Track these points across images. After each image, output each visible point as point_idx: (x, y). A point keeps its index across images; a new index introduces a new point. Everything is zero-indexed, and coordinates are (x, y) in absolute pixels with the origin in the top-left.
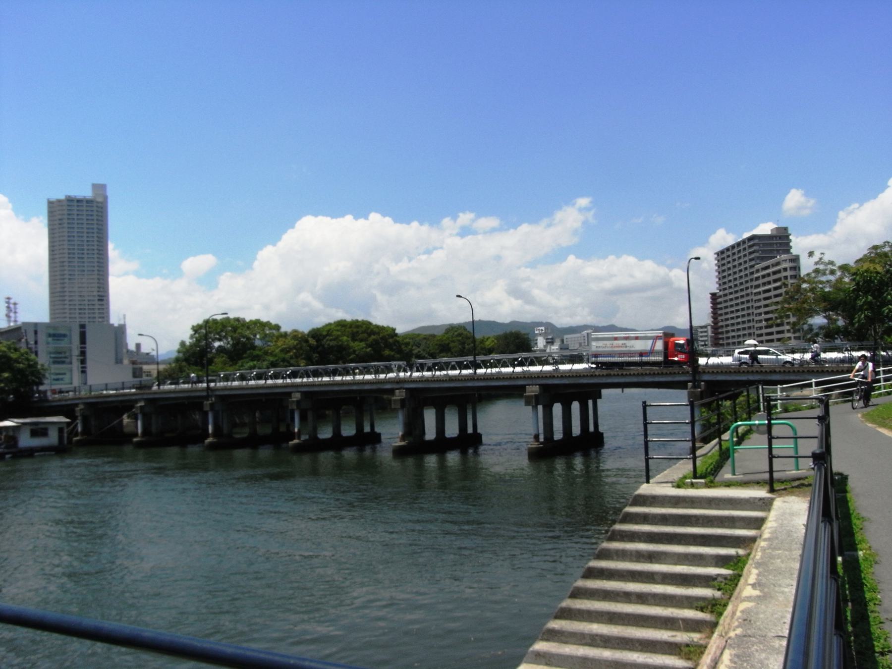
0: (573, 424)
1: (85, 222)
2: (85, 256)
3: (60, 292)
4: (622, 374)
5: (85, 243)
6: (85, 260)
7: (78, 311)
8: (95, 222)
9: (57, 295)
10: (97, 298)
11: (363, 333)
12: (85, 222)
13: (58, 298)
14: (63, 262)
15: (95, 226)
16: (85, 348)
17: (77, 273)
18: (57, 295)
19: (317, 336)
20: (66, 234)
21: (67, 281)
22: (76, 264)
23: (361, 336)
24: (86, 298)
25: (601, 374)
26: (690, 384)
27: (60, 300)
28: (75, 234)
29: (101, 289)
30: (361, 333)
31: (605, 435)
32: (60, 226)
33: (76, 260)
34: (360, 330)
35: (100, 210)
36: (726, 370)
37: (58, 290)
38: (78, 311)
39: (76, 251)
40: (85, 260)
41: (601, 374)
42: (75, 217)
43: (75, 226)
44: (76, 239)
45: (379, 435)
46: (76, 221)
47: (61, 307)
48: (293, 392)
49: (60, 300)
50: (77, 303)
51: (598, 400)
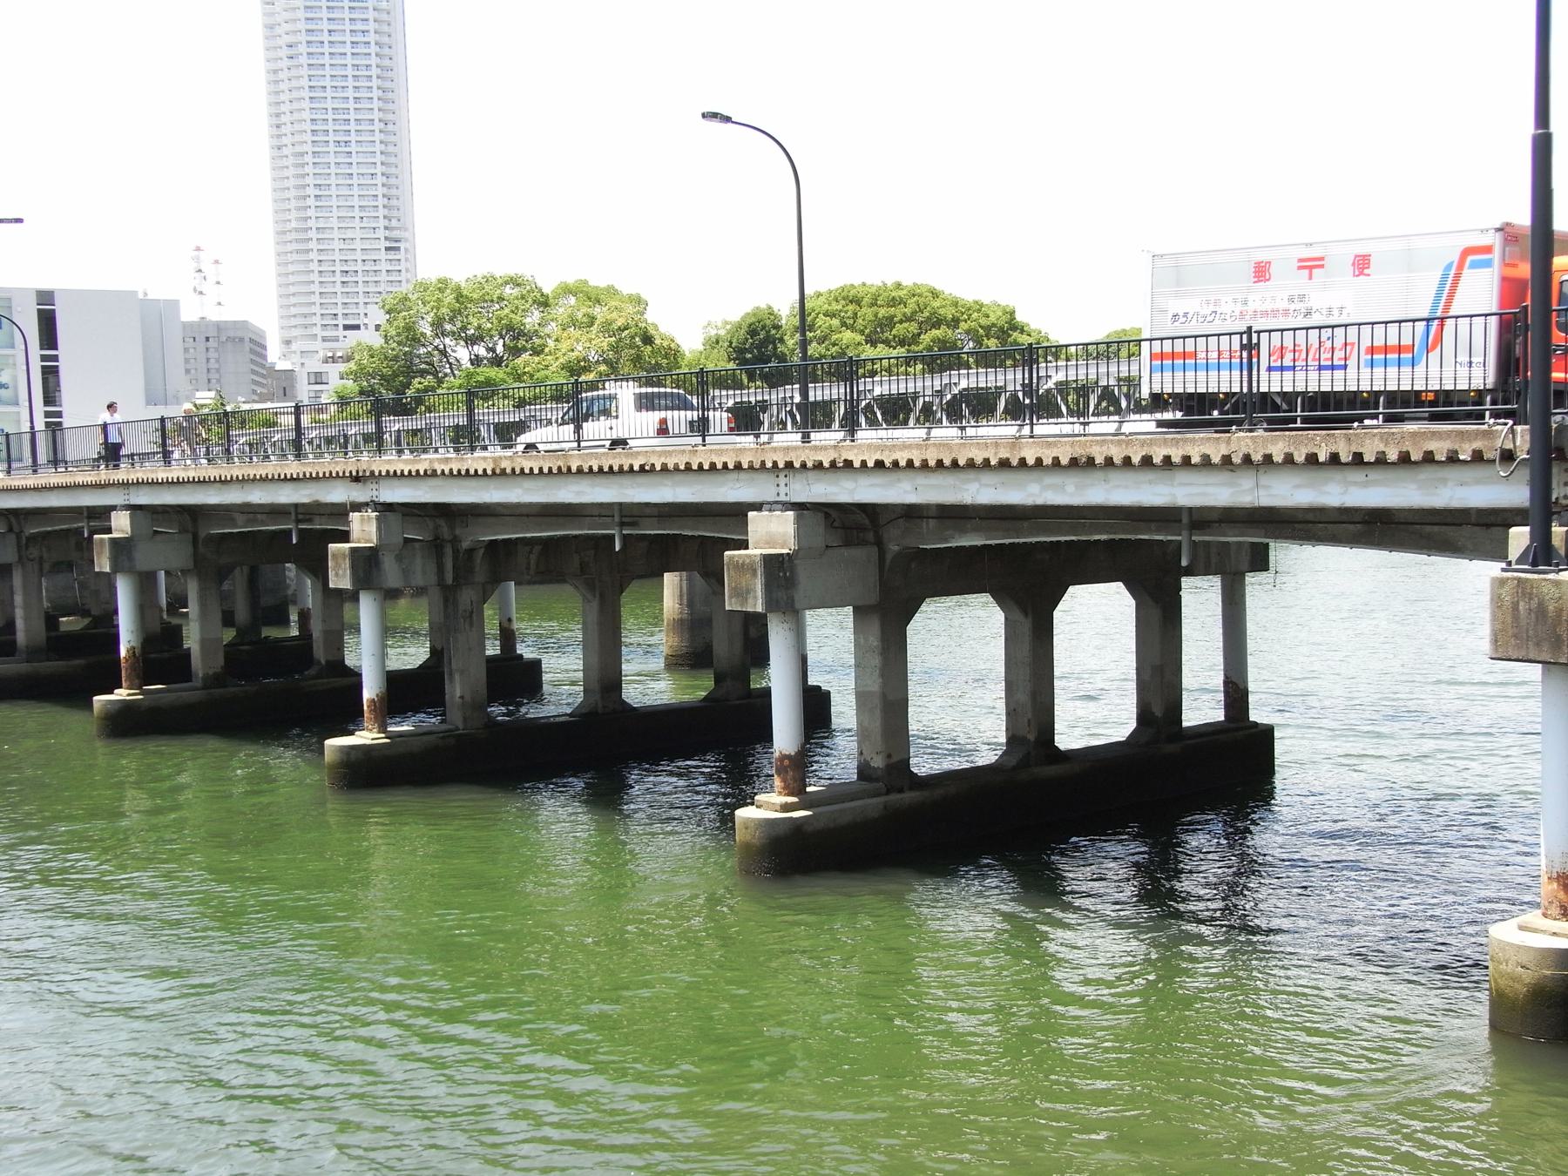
0: (1189, 679)
1: (348, 49)
2: (353, 137)
3: (297, 230)
4: (1312, 460)
5: (351, 105)
6: (353, 148)
7: (339, 278)
8: (373, 49)
9: (289, 237)
10: (384, 244)
11: (909, 319)
12: (348, 49)
13: (295, 246)
14: (302, 154)
15: (374, 61)
16: (55, 358)
17: (333, 181)
18: (289, 237)
19: (764, 327)
20: (305, 82)
21: (311, 202)
22: (332, 159)
23: (899, 329)
24: (358, 245)
25: (979, 460)
26: (1519, 537)
27: (298, 252)
28: (328, 82)
29: (394, 223)
30: (901, 322)
31: (1283, 749)
32: (290, 63)
33: (332, 148)
34: (898, 312)
35: (384, 17)
36: (1004, 454)
37: (294, 224)
38: (339, 278)
39: (330, 127)
40: (353, 148)
41: (979, 460)
42: (326, 37)
43: (326, 60)
44: (329, 93)
45: (535, 666)
46: (326, 49)
47: (302, 267)
48: (114, 508)
49: (298, 252)
50: (337, 256)
51: (1251, 579)
